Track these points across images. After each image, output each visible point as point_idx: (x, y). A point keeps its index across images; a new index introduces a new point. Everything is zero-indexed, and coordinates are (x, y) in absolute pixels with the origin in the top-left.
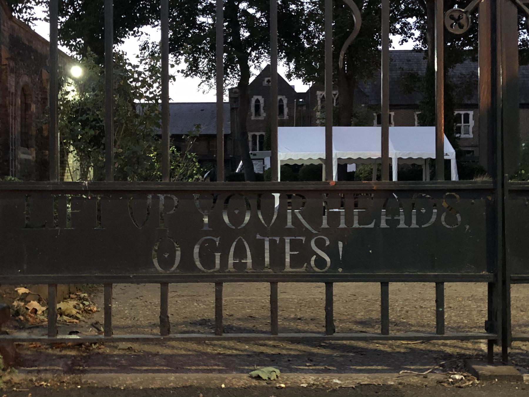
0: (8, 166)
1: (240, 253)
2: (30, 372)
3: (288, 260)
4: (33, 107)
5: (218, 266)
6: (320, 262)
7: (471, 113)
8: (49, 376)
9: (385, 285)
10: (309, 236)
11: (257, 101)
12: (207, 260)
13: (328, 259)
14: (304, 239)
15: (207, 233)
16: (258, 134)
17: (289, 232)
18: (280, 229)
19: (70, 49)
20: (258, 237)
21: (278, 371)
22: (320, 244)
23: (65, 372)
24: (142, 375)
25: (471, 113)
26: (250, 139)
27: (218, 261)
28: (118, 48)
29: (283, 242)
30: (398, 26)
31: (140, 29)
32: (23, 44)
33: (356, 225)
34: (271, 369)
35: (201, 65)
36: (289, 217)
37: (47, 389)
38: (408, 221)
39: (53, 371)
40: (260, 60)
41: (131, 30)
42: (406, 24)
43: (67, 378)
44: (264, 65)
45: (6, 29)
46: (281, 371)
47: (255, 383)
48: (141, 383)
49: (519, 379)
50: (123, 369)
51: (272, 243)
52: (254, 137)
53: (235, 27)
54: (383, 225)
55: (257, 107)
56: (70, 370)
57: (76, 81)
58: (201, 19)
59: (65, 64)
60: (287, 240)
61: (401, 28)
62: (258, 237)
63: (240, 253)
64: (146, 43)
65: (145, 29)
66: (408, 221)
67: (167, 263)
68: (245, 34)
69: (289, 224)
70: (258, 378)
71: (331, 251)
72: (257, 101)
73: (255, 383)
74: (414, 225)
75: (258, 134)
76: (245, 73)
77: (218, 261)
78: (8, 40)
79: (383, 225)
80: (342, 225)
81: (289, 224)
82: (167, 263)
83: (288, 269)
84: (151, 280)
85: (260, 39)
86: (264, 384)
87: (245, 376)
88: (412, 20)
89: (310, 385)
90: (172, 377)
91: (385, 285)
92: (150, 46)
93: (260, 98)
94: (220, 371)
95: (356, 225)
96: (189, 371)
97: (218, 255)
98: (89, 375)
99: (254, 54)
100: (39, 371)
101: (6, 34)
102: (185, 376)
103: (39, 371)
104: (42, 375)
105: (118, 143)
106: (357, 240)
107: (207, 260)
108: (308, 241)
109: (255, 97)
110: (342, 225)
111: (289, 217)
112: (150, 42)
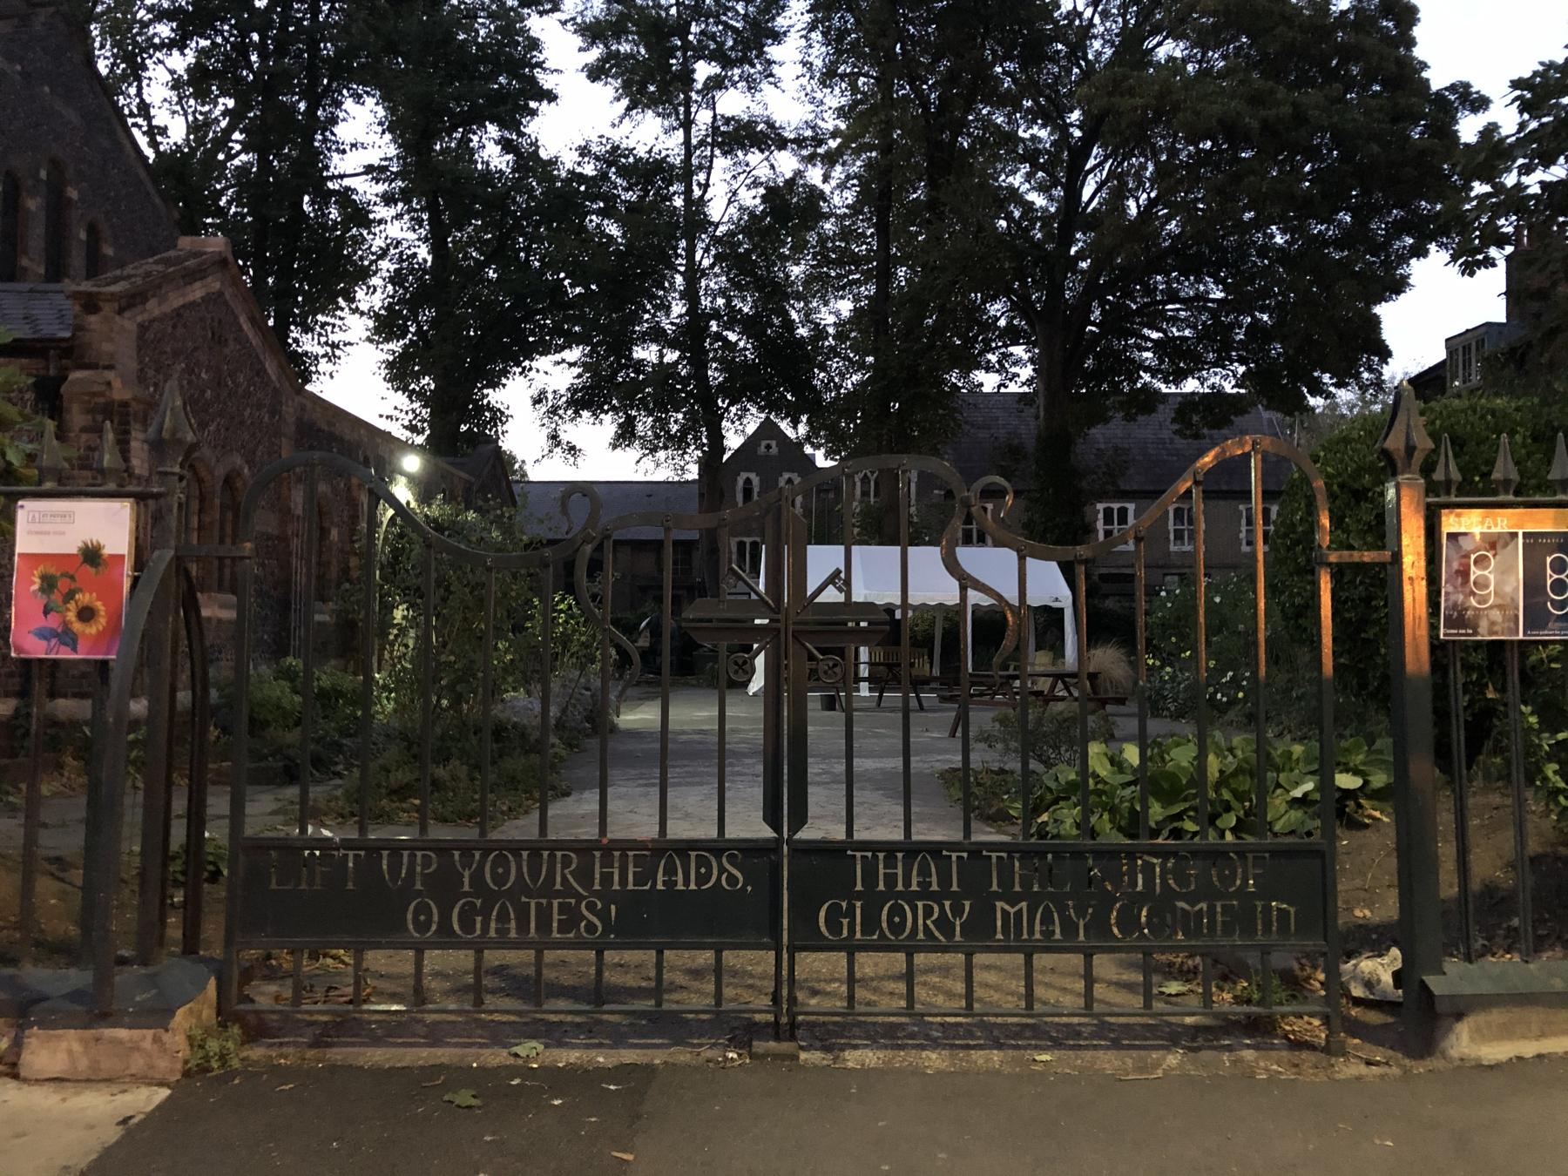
0: (288, 637)
1: (503, 917)
2: (271, 1045)
3: (555, 925)
4: (334, 534)
5: (478, 932)
6: (591, 928)
7: (1131, 507)
8: (291, 1050)
9: (660, 953)
10: (580, 898)
11: (748, 481)
12: (467, 925)
13: (598, 923)
14: (573, 901)
15: (466, 894)
16: (748, 540)
17: (558, 894)
18: (548, 891)
19: (410, 397)
20: (524, 899)
21: (541, 1047)
22: (591, 907)
23: (311, 1046)
24: (393, 1050)
25: (1131, 507)
26: (734, 549)
27: (478, 926)
28: (494, 397)
29: (550, 905)
30: (993, 358)
31: (534, 364)
32: (319, 430)
33: (630, 887)
34: (534, 1043)
35: (640, 427)
36: (559, 879)
37: (287, 1067)
38: (687, 882)
39: (295, 1044)
40: (745, 421)
41: (518, 364)
42: (1006, 356)
43: (310, 1054)
44: (751, 428)
45: (291, 410)
46: (547, 1046)
47: (511, 1061)
48: (388, 1060)
49: (795, 1057)
50: (376, 1041)
51: (538, 905)
52: (741, 545)
53: (699, 363)
54: (660, 887)
55: (748, 492)
56: (316, 1044)
57: (411, 479)
58: (639, 353)
59: (392, 452)
60: (555, 903)
61: (999, 362)
62: (524, 899)
63: (503, 917)
64: (543, 393)
65: (543, 362)
66: (687, 882)
67: (422, 927)
68: (715, 375)
69: (558, 886)
70: (516, 1055)
71: (603, 915)
72: (748, 481)
73: (511, 1061)
74: (693, 887)
75: (748, 540)
76: (717, 438)
77: (478, 926)
78: (293, 428)
79: (660, 887)
80: (616, 887)
81: (558, 886)
82: (422, 927)
83: (555, 935)
84: (405, 946)
85: (744, 385)
86: (520, 1062)
87: (505, 1052)
88: (1019, 351)
89: (568, 1064)
90: (424, 1053)
91: (660, 953)
92: (550, 396)
93: (753, 476)
94: (482, 1046)
95: (630, 887)
96: (448, 1045)
97: (479, 919)
98: (335, 1050)
99: (733, 409)
100: (281, 1044)
101: (291, 420)
102: (439, 1051)
103: (281, 1044)
104: (284, 1050)
105: (449, 647)
106: (632, 903)
107: (467, 925)
108: (578, 903)
109: (744, 475)
110: (616, 887)
111: (559, 879)
112: (550, 390)
